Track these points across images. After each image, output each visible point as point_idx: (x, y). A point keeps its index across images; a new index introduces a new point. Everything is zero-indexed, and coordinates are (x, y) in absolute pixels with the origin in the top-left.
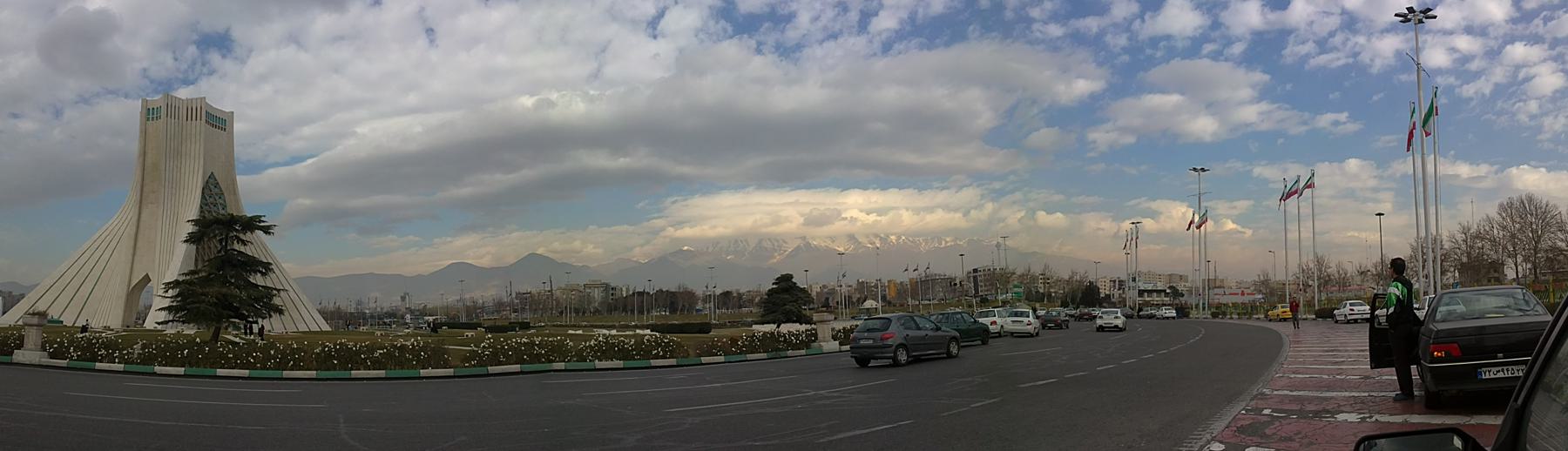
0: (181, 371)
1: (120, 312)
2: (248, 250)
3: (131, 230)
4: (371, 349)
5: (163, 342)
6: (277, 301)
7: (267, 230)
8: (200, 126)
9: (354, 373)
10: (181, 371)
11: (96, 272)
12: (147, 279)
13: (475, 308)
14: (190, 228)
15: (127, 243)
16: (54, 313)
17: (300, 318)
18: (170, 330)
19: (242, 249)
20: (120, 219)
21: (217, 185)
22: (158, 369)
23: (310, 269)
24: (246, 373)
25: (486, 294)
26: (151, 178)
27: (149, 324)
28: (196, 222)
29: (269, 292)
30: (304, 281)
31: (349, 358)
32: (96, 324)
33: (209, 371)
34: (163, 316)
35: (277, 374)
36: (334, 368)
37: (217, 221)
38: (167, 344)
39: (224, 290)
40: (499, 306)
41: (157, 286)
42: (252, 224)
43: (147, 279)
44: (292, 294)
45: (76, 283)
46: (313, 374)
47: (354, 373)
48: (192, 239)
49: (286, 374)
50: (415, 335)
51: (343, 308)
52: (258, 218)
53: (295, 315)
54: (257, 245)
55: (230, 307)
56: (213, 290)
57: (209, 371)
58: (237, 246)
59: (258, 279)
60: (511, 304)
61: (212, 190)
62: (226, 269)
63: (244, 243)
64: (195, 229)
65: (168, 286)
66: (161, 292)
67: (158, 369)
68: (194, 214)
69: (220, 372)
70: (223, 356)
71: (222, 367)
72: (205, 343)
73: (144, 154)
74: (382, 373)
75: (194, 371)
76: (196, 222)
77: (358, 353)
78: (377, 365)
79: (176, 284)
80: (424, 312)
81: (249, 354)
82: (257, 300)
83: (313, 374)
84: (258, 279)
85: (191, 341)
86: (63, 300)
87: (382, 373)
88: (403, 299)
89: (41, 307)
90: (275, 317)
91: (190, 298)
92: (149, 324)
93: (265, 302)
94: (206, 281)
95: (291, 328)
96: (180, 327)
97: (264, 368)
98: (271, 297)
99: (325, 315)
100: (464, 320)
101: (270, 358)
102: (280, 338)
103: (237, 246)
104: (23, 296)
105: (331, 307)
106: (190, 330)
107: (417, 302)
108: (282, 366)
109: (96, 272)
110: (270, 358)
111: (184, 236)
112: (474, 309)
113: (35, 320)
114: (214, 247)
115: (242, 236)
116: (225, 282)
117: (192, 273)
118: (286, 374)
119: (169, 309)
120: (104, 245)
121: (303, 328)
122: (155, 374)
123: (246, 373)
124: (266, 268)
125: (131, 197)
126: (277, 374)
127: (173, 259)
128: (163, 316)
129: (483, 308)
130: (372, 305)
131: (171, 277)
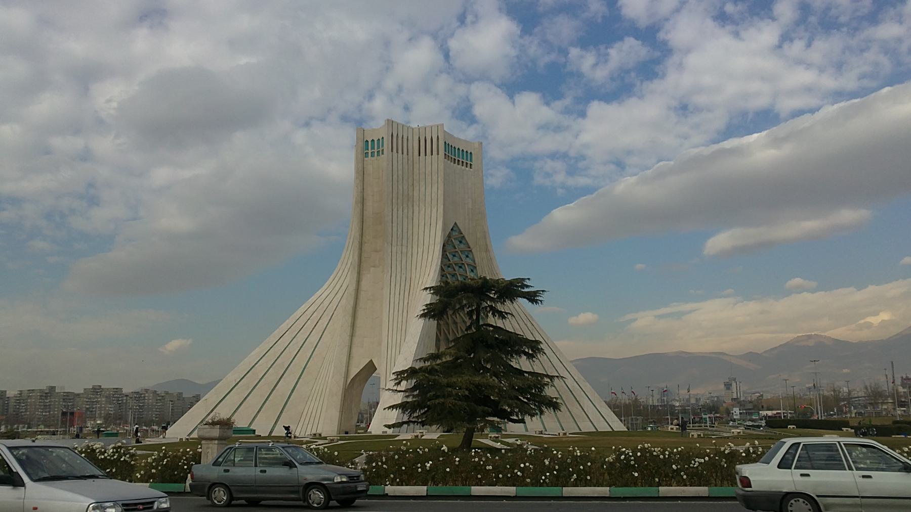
0: (422, 490)
1: (334, 413)
2: (508, 325)
3: (347, 303)
4: (686, 457)
5: (397, 451)
6: (549, 392)
7: (533, 297)
8: (436, 163)
9: (664, 490)
10: (422, 490)
11: (300, 361)
12: (370, 368)
13: (837, 399)
14: (428, 298)
15: (341, 322)
16: (241, 422)
17: (584, 413)
18: (406, 435)
19: (499, 323)
20: (335, 289)
21: (462, 239)
22: (390, 489)
23: (593, 339)
24: (511, 490)
25: (853, 382)
26: (374, 230)
27: (377, 427)
28: (436, 290)
29: (538, 381)
30: (591, 367)
31: (655, 470)
32: (301, 431)
33: (460, 490)
34: (394, 416)
35: (554, 491)
36: (634, 483)
37: (465, 288)
38: (402, 454)
39: (477, 379)
40: (876, 396)
41: (385, 376)
42: (512, 290)
43: (370, 368)
44: (570, 381)
45: (272, 377)
46: (604, 491)
47: (664, 490)
48: (431, 312)
49: (568, 491)
50: (751, 438)
51: (642, 399)
52: (520, 283)
53: (576, 410)
54: (519, 318)
55: (486, 401)
56: (463, 379)
57: (460, 490)
58: (492, 320)
59: (522, 363)
60: (895, 395)
61: (455, 245)
62: (478, 352)
63: (502, 315)
64: (436, 299)
65: (401, 376)
66: (391, 385)
67: (390, 489)
68: (431, 277)
69: (476, 490)
70: (478, 468)
71: (479, 483)
72: (453, 450)
73: (362, 201)
74: (703, 491)
75: (441, 489)
76: (436, 290)
77: (667, 462)
78: (696, 478)
79: (411, 373)
80: (758, 405)
81: (515, 465)
82: (522, 391)
83: (604, 491)
84: (522, 363)
85: (434, 450)
86: (255, 401)
87: (703, 491)
88: (728, 386)
89: (223, 413)
90: (548, 413)
91: (429, 394)
92: (377, 427)
93: (533, 395)
94: (453, 367)
95: (570, 428)
96: (418, 431)
97: (536, 483)
98: (541, 386)
99: (619, 410)
100: (820, 416)
101: (543, 469)
102: (558, 442)
103: (492, 320)
104: (197, 399)
105: (625, 399)
106: (432, 434)
107: (744, 390)
108: (561, 480)
109: (300, 361)
110: (543, 469)
111: (420, 308)
112: (833, 401)
113: (216, 432)
114: (461, 322)
115: (500, 307)
116: (478, 368)
117: (433, 357)
118: (568, 491)
119: (403, 406)
120: (310, 325)
121: (587, 427)
122: (386, 496)
123: (511, 490)
124: (533, 348)
125: (348, 257)
126: (554, 491)
127: (404, 340)
128: (394, 416)
129: (849, 399)
130: (683, 392)
131: (405, 361)
